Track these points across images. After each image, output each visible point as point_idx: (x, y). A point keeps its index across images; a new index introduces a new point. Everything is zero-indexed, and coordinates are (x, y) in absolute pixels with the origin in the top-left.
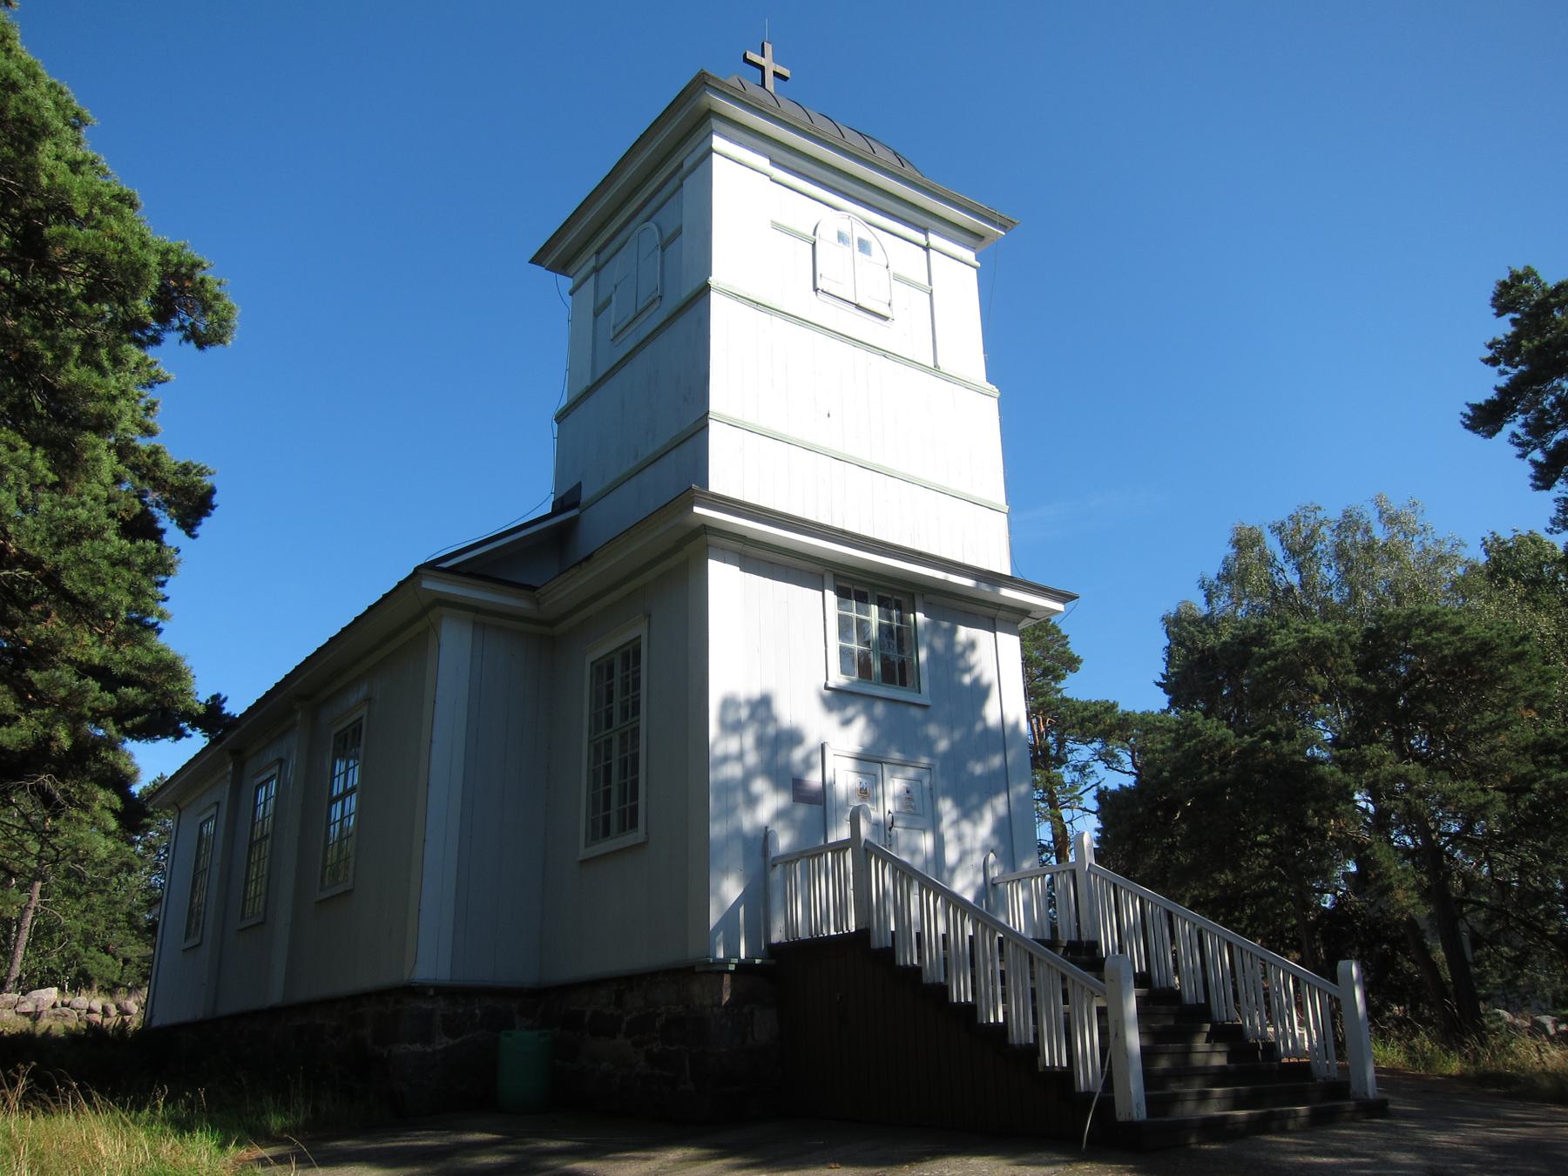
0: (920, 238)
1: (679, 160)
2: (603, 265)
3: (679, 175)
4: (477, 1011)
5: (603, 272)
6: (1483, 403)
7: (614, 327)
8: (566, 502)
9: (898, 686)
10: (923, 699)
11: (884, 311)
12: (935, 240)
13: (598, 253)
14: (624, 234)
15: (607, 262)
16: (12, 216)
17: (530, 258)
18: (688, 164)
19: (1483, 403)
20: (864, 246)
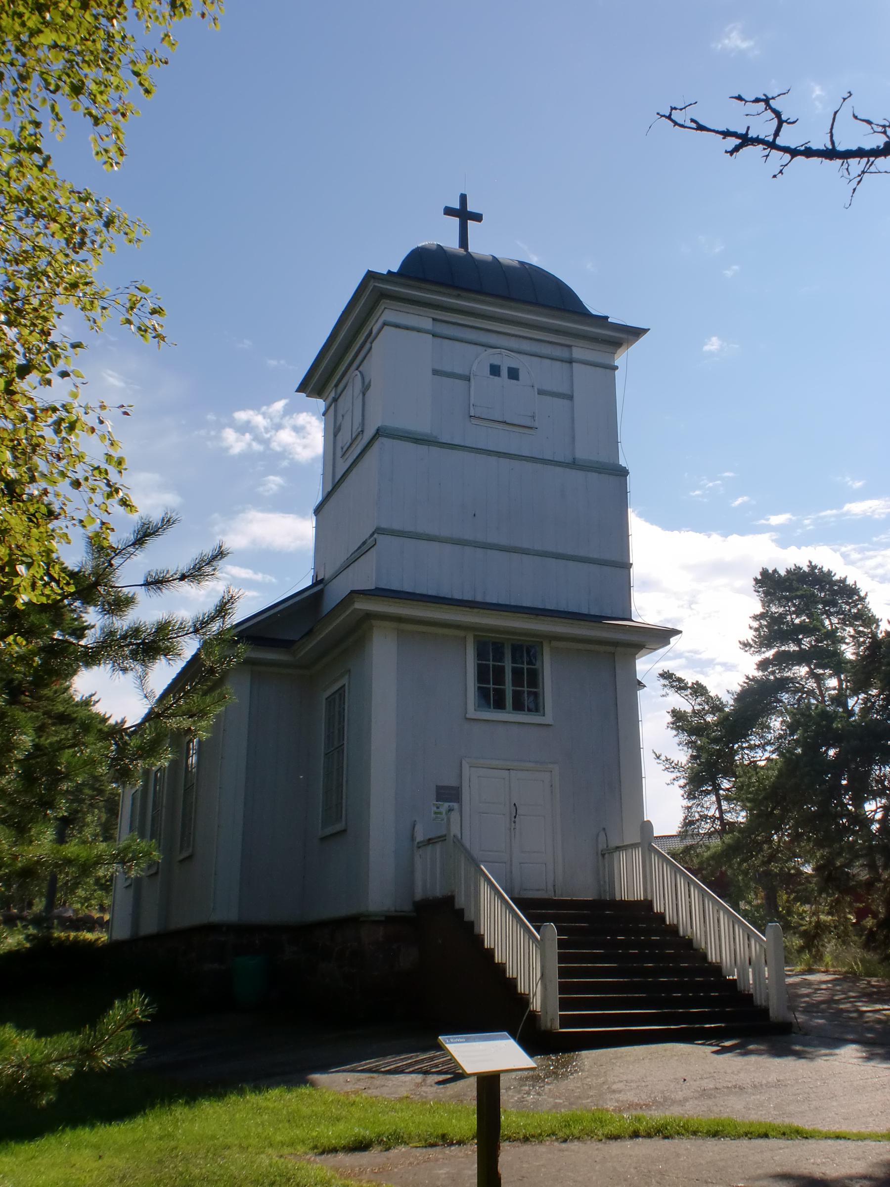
0: (558, 352)
1: (370, 328)
2: (340, 395)
3: (370, 340)
4: (257, 942)
5: (340, 400)
6: (783, 573)
7: (342, 448)
8: (317, 582)
9: (526, 712)
10: (548, 719)
11: (528, 422)
12: (578, 353)
13: (336, 386)
14: (368, 346)
15: (342, 392)
16: (44, 18)
17: (297, 386)
18: (375, 331)
19: (783, 573)
20: (513, 374)
